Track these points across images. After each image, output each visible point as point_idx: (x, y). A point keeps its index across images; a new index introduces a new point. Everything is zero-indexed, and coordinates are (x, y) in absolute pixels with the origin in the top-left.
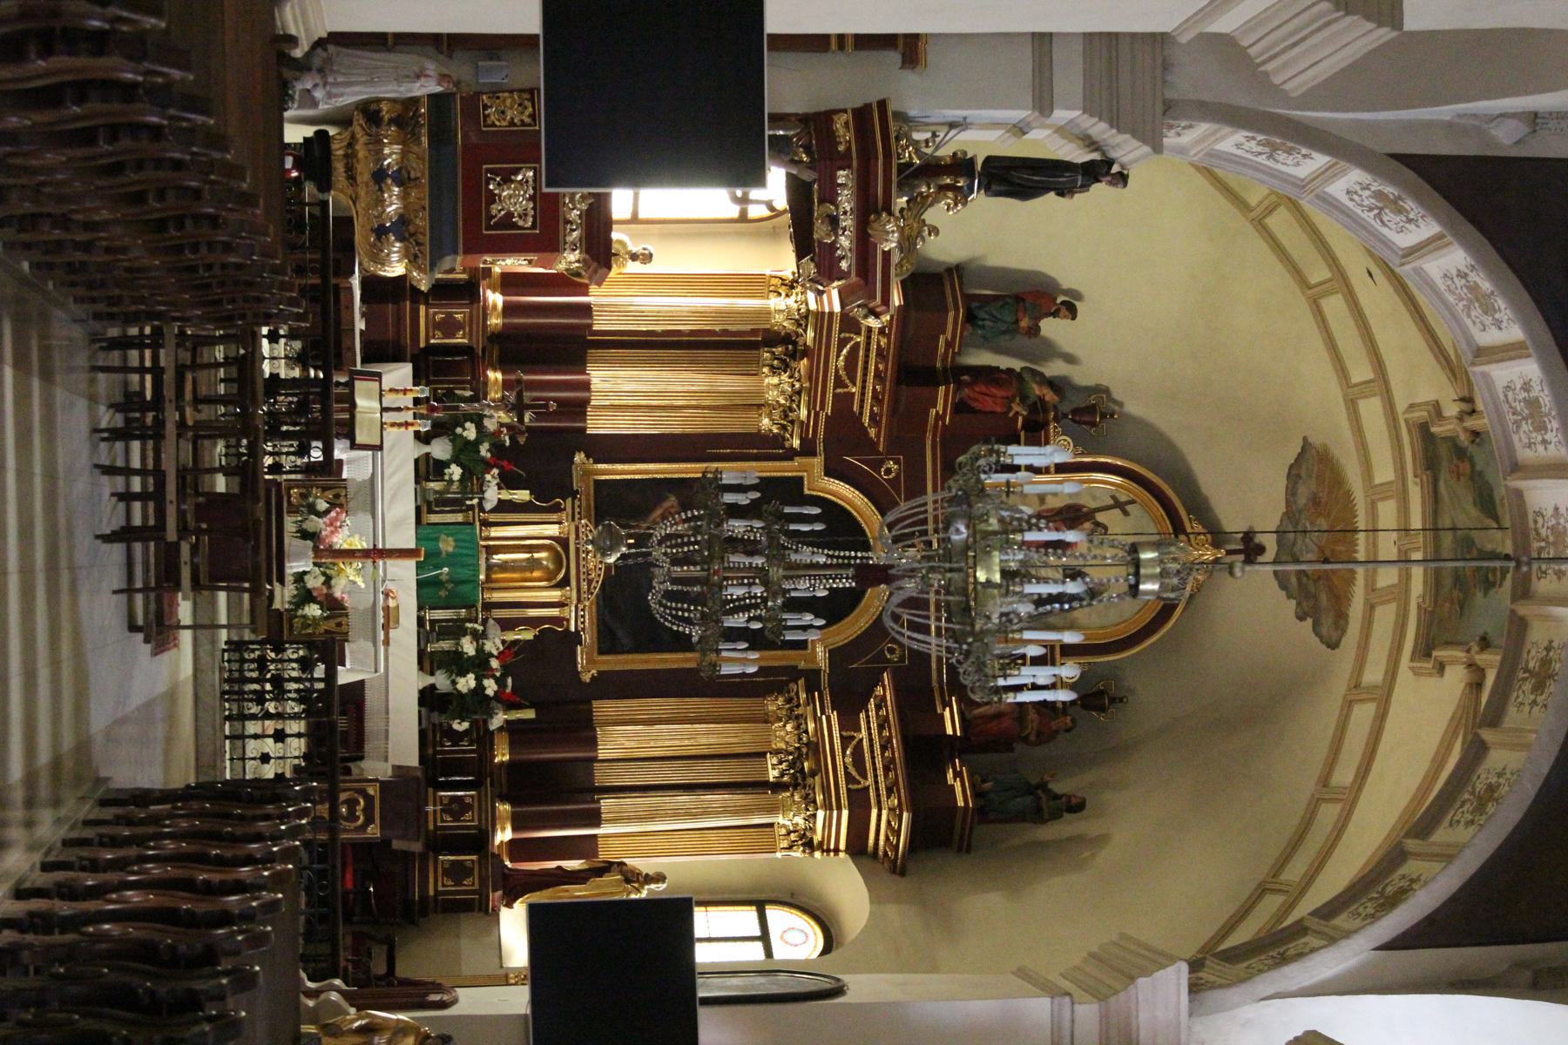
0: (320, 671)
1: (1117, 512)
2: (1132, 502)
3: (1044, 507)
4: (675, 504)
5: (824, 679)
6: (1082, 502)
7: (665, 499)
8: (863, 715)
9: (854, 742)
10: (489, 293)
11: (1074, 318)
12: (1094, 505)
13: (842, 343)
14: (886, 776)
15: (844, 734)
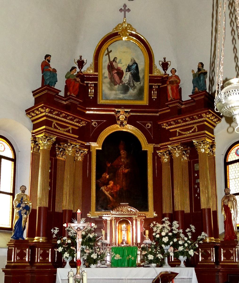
0: (128, 257)
1: (110, 54)
2: (107, 49)
3: (108, 77)
4: (103, 187)
5: (156, 146)
6: (107, 65)
7: (102, 190)
8: (171, 131)
9: (181, 132)
11: (51, 56)
12: (108, 61)
13: (55, 127)
15: (177, 135)
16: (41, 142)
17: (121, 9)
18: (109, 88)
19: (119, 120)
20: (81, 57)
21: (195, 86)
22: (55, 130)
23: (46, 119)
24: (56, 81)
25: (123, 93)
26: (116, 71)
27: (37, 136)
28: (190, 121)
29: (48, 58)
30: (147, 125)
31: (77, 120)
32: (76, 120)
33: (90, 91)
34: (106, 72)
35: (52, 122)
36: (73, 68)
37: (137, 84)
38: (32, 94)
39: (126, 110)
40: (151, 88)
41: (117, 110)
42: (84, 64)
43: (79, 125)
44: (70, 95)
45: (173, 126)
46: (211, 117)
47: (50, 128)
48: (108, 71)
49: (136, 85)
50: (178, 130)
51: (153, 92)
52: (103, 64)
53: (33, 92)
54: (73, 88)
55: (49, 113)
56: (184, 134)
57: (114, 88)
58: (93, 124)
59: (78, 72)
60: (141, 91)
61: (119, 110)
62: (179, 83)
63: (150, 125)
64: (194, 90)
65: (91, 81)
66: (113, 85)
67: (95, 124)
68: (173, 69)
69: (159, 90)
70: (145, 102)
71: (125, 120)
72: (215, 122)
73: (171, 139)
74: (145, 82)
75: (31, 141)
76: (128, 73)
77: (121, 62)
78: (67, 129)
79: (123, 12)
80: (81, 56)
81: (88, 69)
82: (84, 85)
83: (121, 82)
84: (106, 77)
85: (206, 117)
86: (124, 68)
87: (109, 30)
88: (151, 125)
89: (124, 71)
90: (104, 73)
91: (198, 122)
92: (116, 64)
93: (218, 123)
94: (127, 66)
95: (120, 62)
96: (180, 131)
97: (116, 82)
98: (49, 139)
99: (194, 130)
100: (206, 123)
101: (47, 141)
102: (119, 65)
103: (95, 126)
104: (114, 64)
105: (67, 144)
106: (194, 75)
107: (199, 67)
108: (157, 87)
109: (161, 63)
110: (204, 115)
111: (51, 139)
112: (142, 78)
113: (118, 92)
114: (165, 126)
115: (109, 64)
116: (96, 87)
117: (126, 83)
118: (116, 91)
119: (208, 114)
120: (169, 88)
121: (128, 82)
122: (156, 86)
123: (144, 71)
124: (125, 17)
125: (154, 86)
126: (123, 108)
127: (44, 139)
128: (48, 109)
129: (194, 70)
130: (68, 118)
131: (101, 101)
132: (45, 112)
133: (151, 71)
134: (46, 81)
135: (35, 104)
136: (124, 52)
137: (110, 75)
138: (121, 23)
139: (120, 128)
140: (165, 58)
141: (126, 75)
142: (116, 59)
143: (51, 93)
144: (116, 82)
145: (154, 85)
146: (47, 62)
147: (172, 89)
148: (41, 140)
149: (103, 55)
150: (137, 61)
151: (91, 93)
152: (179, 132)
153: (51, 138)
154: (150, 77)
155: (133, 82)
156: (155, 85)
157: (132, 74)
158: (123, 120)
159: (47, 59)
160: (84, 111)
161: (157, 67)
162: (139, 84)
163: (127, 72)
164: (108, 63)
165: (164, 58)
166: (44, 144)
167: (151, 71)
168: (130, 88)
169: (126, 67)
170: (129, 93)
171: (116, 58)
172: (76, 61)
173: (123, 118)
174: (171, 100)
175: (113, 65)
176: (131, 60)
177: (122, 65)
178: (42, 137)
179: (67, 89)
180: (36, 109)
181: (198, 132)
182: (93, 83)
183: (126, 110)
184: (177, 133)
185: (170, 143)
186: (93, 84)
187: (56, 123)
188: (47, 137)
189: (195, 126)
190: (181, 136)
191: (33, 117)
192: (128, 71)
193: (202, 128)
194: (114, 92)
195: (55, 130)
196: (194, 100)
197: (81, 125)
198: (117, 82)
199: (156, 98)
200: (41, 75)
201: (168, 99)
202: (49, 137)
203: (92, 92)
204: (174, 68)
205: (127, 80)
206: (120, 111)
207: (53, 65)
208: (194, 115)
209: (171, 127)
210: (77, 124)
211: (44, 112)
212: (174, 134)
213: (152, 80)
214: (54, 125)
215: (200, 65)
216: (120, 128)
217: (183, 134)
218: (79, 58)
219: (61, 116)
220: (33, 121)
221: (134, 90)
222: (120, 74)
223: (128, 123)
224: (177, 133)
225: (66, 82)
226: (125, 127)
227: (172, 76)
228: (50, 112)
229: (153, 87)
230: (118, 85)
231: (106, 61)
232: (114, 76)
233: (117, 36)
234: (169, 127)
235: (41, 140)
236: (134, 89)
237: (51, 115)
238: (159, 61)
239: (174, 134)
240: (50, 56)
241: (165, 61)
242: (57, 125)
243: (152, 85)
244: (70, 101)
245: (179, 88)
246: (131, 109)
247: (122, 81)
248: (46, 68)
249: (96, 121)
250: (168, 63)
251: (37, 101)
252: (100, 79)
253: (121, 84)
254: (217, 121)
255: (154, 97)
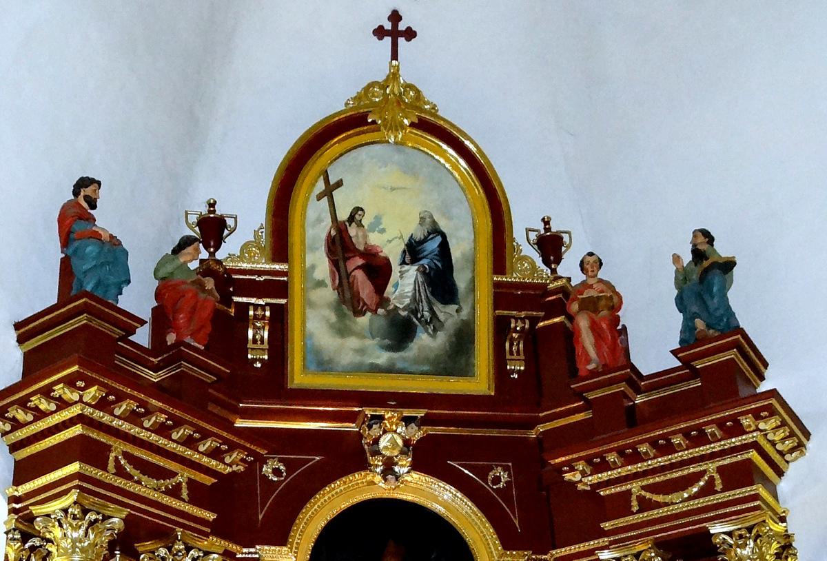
3: (329, 281)
6: (324, 236)
9: (648, 495)
10: (428, 368)
11: (99, 183)
12: (328, 222)
13: (120, 472)
14: (678, 448)
15: (635, 509)
16: (57, 532)
17: (381, 27)
18: (332, 326)
19: (377, 453)
20: (212, 205)
21: (695, 313)
22: (120, 482)
23: (81, 436)
24: (125, 282)
25: (390, 348)
26: (360, 262)
27: (36, 510)
28: (687, 449)
29: (88, 191)
30: (491, 474)
31: (215, 444)
32: (208, 444)
33: (254, 336)
34: (319, 263)
35: (108, 448)
36: (185, 243)
37: (446, 313)
38: (13, 335)
39: (407, 413)
40: (501, 328)
41: (369, 412)
42: (226, 232)
43: (220, 467)
44: (179, 343)
45: (717, 447)
46: (775, 434)
47: (98, 474)
48: (327, 259)
49: (441, 316)
50: (635, 487)
51: (511, 345)
52: (310, 232)
53: (17, 326)
54: (190, 320)
55: (95, 407)
56: (666, 504)
57: (357, 328)
58: (267, 470)
59: (202, 261)
60: (463, 339)
61: (381, 412)
62: (619, 308)
63: (504, 477)
64: (688, 328)
65: (259, 297)
66: (350, 313)
67: (276, 472)
68: (591, 254)
69: (532, 338)
70: (480, 383)
71: (402, 453)
72: (781, 453)
73: (607, 526)
74: (477, 307)
75: (7, 533)
76: (408, 271)
77: (381, 227)
78: (170, 483)
79: (388, 40)
80: (212, 201)
81: (245, 247)
82: (228, 314)
83: (383, 301)
84: (320, 284)
85: (758, 429)
86: (393, 251)
87: (334, 104)
88: (509, 476)
89: (395, 262)
90: (313, 267)
91: (723, 453)
92: (360, 234)
93: (793, 461)
94: (406, 241)
95: (377, 224)
96: (643, 493)
97: (361, 304)
98: (96, 521)
99: (707, 482)
100: (753, 455)
101: (87, 529)
102: (375, 239)
103: (276, 479)
104: (352, 231)
105: (170, 549)
106: (682, 278)
107: (699, 247)
108: (527, 326)
109: (533, 236)
110: (746, 421)
111: (103, 520)
112: (465, 288)
113: (369, 342)
114: (580, 477)
115: (333, 233)
116: (280, 319)
117: (401, 306)
118: (360, 336)
119: (766, 417)
120: (583, 323)
121: (409, 305)
122: (523, 320)
123: (472, 262)
124: (395, 56)
125: (516, 319)
126: (391, 406)
127: (75, 518)
128: (96, 387)
129: (679, 257)
130: (175, 436)
131: (299, 377)
132: (81, 401)
133: (500, 260)
134: (81, 276)
135: (25, 373)
136: (393, 189)
137: (335, 276)
138: (380, 81)
139: (383, 485)
140: (548, 218)
141: (401, 277)
142: (360, 212)
143: (106, 327)
144: (361, 304)
145: (513, 317)
146: (85, 205)
147: (594, 327)
148: (57, 523)
149: (307, 199)
150: (443, 225)
151: (259, 345)
152: (641, 500)
153: (106, 518)
154: (497, 285)
155: (429, 303)
156: (521, 318)
157: (423, 272)
158: (396, 453)
159: (82, 194)
160: (231, 417)
161: (521, 250)
162: (455, 314)
163: (408, 264)
164: (329, 227)
165: (543, 219)
166: (74, 541)
167: (500, 260)
168: (420, 328)
169: (403, 247)
170: (416, 347)
171: (362, 210)
172: (193, 219)
173: (395, 444)
174: (594, 373)
175: (351, 237)
176: (421, 218)
177: (386, 237)
178: (65, 511)
179: (162, 321)
180: (40, 388)
181: (727, 494)
182: (267, 304)
183: (407, 413)
184: (634, 498)
185: (605, 540)
186: (268, 308)
187: (126, 455)
188: (85, 512)
189: (711, 467)
190: (744, 490)
191: (17, 425)
192: (408, 259)
193: (740, 475)
194: (353, 342)
195: (120, 482)
196: (693, 369)
197: (229, 470)
198: (365, 304)
199: (522, 368)
200: (55, 254)
201: (577, 370)
202: (98, 513)
203: (262, 342)
204: (581, 259)
205: (407, 297)
206: (381, 418)
207: (106, 219)
208: (641, 442)
209: (605, 476)
210: (213, 463)
211: (76, 403)
212: (621, 505)
213: (504, 296)
214: (117, 460)
215: (701, 239)
216: (383, 485)
217: (659, 505)
218: (204, 210)
219: (147, 424)
220: (14, 448)
221: (433, 336)
222: (378, 270)
223: (415, 467)
224: (631, 501)
225: (158, 295)
226: (402, 483)
227: (584, 285)
228: (102, 405)
229: (513, 325)
230: (369, 314)
231: (319, 220)
232: (351, 280)
233: (361, 129)
234: (594, 479)
235: (61, 525)
236: (435, 330)
237: (106, 419)
238: (528, 230)
239: (621, 505)
240: (96, 185)
241: (550, 229)
242: (129, 463)
243: (509, 318)
244: (179, 367)
245: (619, 327)
246: (426, 410)
247: (388, 300)
248: (79, 227)
249: (280, 460)
250: (562, 238)
251: (35, 365)
252: (297, 287)
253: (380, 311)
254: (792, 450)
255: (516, 366)
